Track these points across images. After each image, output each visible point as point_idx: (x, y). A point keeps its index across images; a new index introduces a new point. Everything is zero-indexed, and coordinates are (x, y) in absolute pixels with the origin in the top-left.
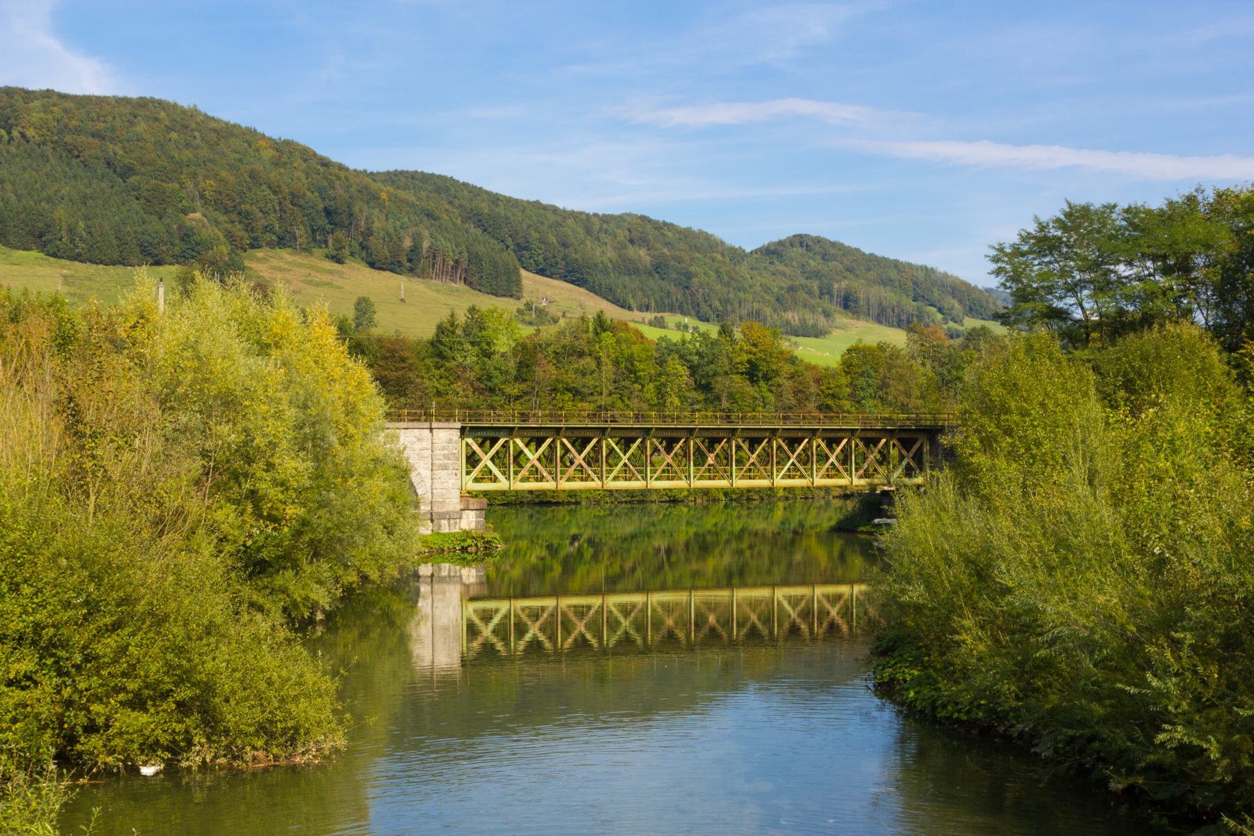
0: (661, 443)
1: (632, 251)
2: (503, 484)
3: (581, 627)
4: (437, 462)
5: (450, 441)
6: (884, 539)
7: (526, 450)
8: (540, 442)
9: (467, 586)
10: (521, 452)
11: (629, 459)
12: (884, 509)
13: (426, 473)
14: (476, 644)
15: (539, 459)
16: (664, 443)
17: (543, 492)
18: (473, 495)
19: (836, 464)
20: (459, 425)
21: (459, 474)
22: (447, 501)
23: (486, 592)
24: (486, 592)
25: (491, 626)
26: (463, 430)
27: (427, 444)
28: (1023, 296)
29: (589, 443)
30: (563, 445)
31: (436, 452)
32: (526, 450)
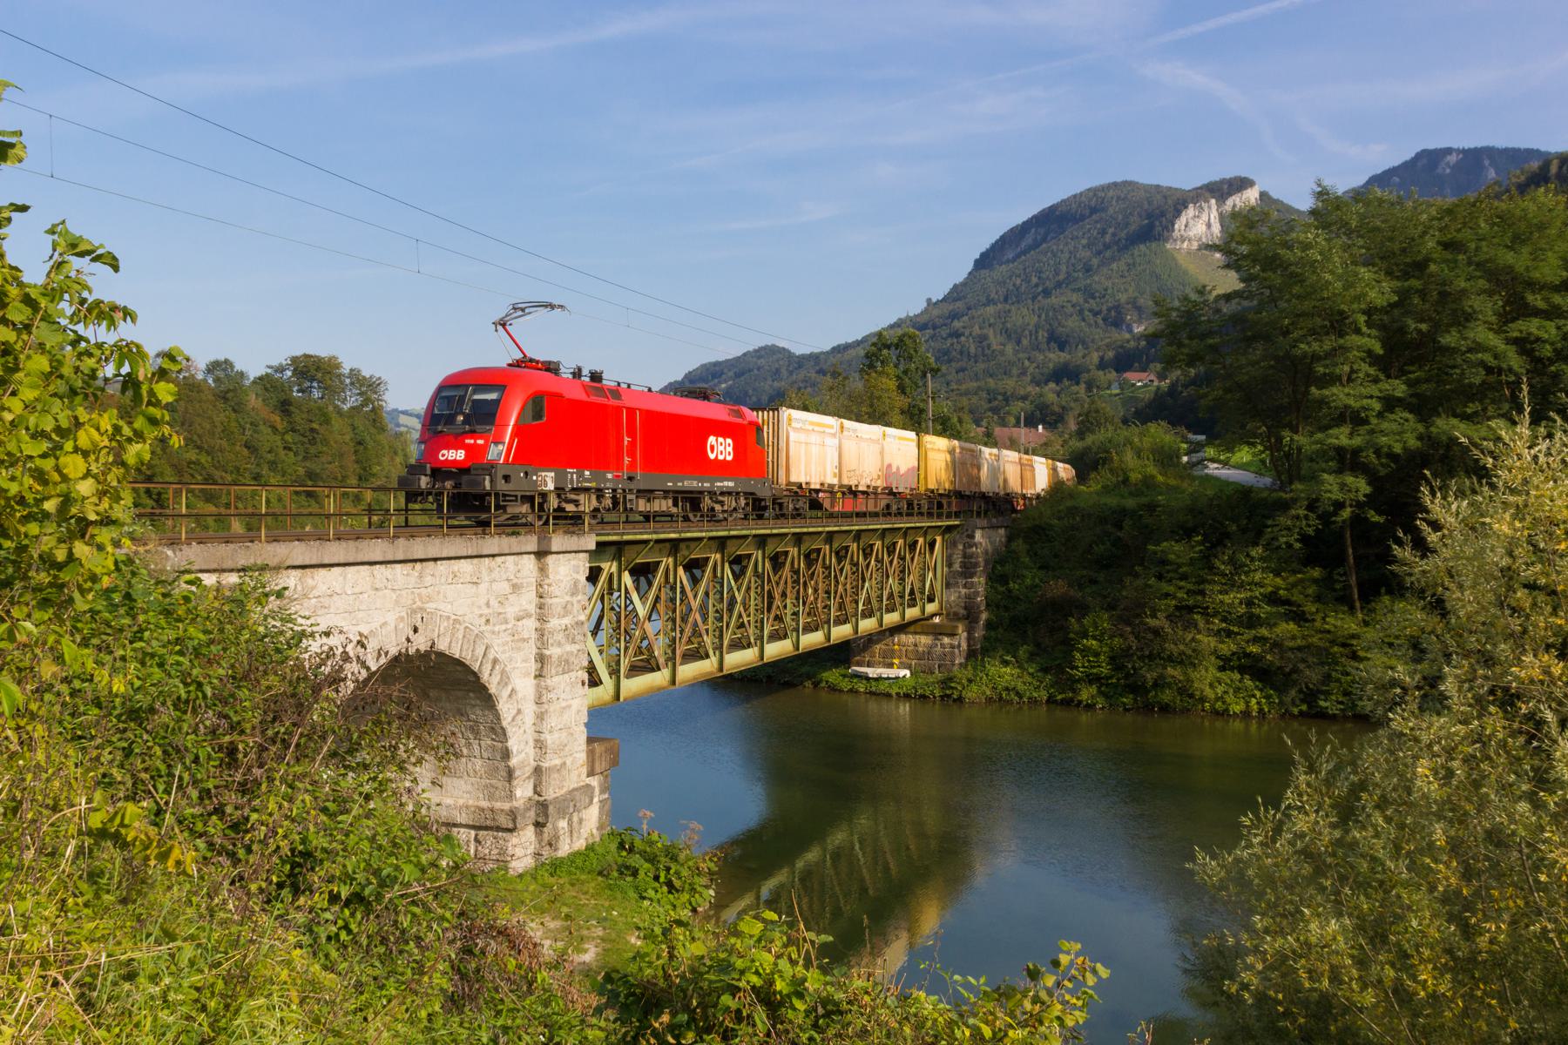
4: (553, 651)
13: (524, 685)
22: (568, 763)
27: (528, 600)
31: (555, 623)
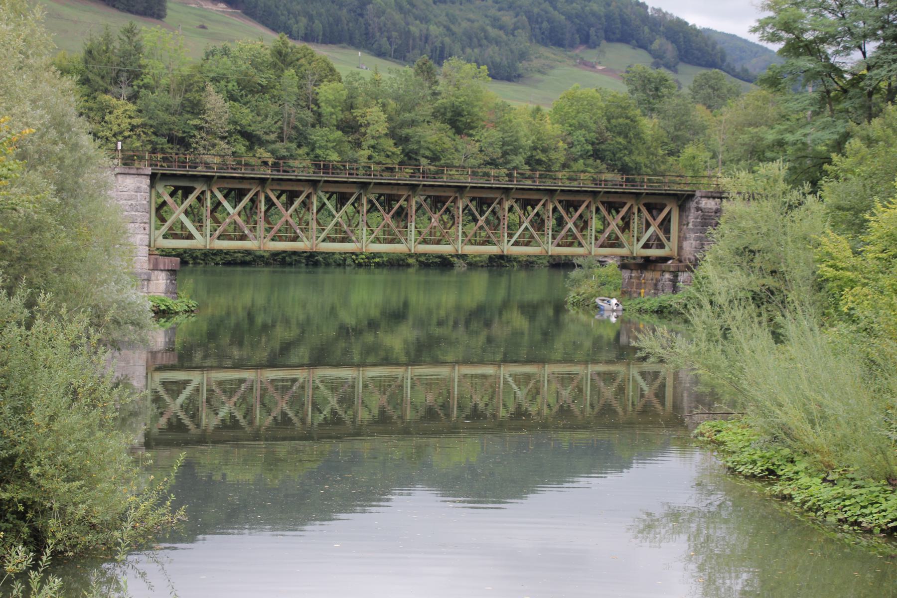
0: (278, 198)
1: (505, 148)
2: (200, 242)
3: (283, 405)
5: (138, 190)
6: (680, 545)
7: (226, 204)
8: (241, 194)
9: (153, 354)
10: (219, 203)
11: (575, 224)
12: (758, 568)
14: (163, 421)
15: (239, 214)
16: (284, 197)
17: (248, 252)
18: (167, 253)
19: (574, 230)
20: (149, 171)
21: (147, 228)
23: (174, 361)
24: (174, 361)
25: (182, 398)
26: (153, 177)
28: (796, 48)
29: (245, 195)
30: (268, 200)
32: (226, 204)
